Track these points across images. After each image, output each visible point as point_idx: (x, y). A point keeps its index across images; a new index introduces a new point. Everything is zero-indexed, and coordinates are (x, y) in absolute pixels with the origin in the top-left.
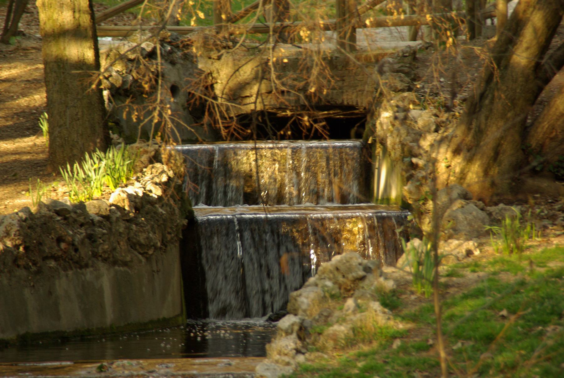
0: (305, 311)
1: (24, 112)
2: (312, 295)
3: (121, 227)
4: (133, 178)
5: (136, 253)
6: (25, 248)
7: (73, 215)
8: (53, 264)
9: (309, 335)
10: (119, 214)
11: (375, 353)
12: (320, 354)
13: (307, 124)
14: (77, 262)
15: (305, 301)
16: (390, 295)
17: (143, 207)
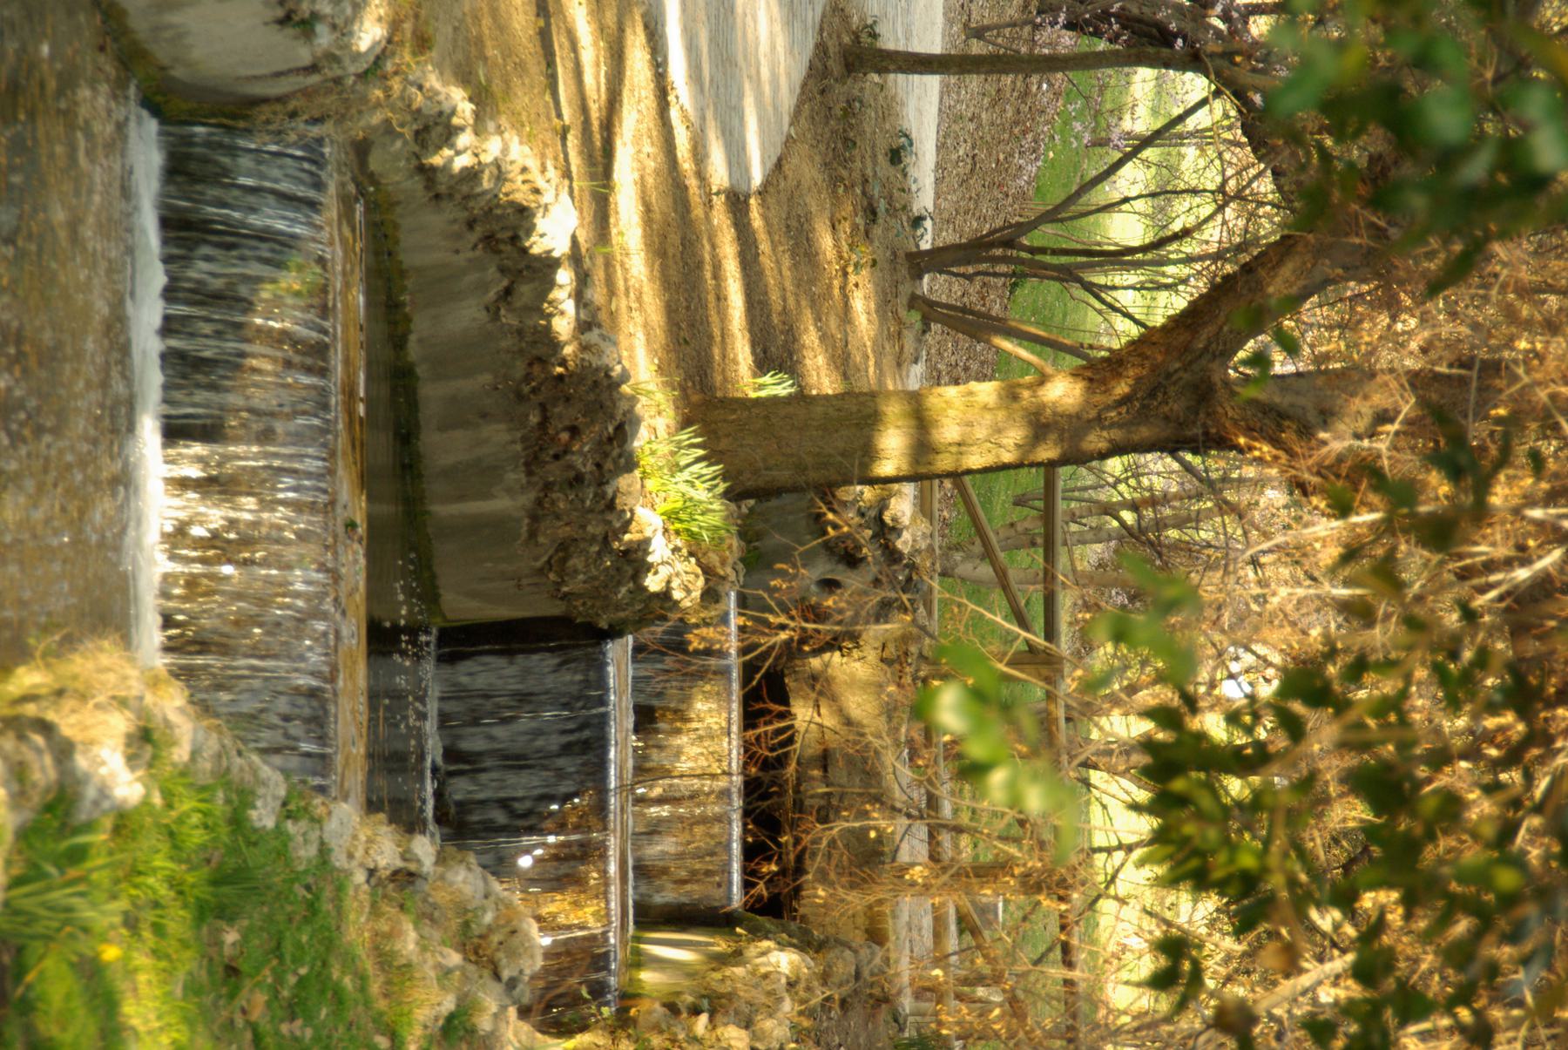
0: (442, 877)
1: (795, 340)
2: (468, 890)
3: (594, 529)
4: (679, 542)
5: (551, 552)
6: (560, 377)
7: (615, 452)
8: (534, 419)
9: (401, 889)
10: (617, 525)
11: (367, 1004)
12: (367, 910)
13: (764, 870)
14: (536, 458)
15: (460, 878)
16: (468, 1025)
17: (630, 562)
